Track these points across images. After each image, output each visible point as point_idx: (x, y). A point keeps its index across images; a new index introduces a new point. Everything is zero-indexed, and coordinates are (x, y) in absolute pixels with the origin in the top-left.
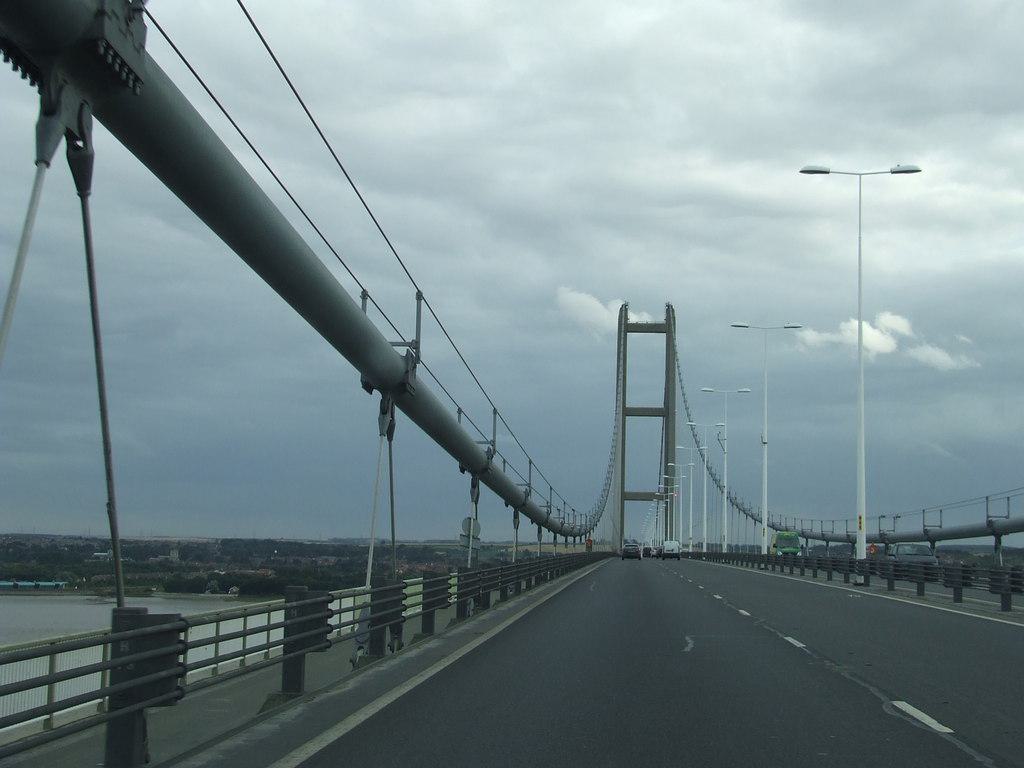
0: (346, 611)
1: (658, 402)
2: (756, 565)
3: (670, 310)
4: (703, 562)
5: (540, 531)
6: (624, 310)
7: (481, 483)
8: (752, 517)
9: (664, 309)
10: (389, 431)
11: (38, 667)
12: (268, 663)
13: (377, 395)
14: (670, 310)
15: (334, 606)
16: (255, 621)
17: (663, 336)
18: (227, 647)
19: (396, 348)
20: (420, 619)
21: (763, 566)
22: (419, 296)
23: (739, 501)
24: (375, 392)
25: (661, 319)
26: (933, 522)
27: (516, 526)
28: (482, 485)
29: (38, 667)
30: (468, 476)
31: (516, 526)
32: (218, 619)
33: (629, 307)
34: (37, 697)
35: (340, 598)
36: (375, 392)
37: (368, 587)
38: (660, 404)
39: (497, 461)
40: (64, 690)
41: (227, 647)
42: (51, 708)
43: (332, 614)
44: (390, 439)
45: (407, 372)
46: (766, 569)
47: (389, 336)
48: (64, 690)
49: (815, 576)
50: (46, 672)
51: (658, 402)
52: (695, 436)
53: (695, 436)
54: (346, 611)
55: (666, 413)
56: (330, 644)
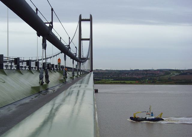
1: (89, 37)
3: (91, 16)
6: (80, 16)
9: (90, 15)
10: (44, 47)
11: (7, 59)
13: (41, 37)
14: (91, 16)
19: (46, 24)
22: (52, 10)
24: (41, 36)
25: (89, 18)
26: (31, 59)
29: (7, 59)
30: (72, 60)
36: (41, 36)
44: (45, 49)
45: (49, 29)
47: (45, 21)
55: (91, 39)
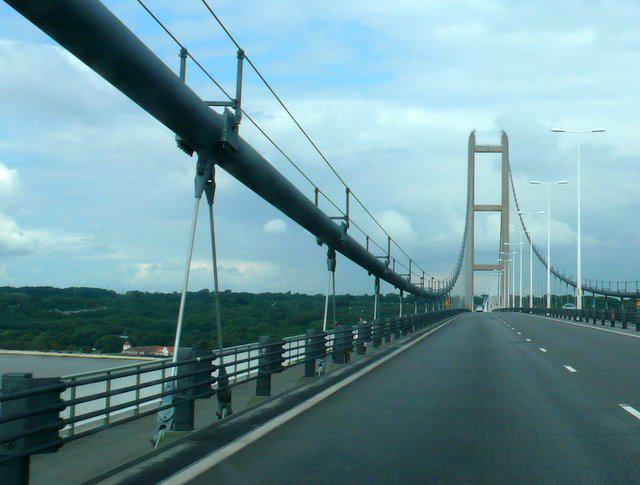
0: (295, 350)
2: (572, 318)
3: (505, 137)
4: (520, 313)
5: (377, 283)
7: (217, 167)
8: (565, 280)
11: (101, 387)
12: (298, 363)
14: (505, 137)
15: (285, 347)
16: (241, 357)
17: (499, 155)
18: (241, 367)
20: (303, 367)
21: (578, 319)
22: (241, 55)
23: (561, 273)
24: (195, 154)
27: (333, 268)
28: (339, 256)
30: (373, 277)
31: (333, 268)
32: (139, 372)
33: (476, 134)
34: (101, 404)
35: (290, 342)
37: (173, 352)
38: (498, 202)
39: (245, 131)
40: (145, 393)
41: (241, 367)
42: (138, 402)
43: (284, 351)
46: (581, 320)
48: (145, 393)
49: (595, 323)
50: (104, 390)
51: (498, 202)
52: (526, 234)
53: (526, 234)
54: (295, 350)
55: (503, 209)
56: (284, 368)
